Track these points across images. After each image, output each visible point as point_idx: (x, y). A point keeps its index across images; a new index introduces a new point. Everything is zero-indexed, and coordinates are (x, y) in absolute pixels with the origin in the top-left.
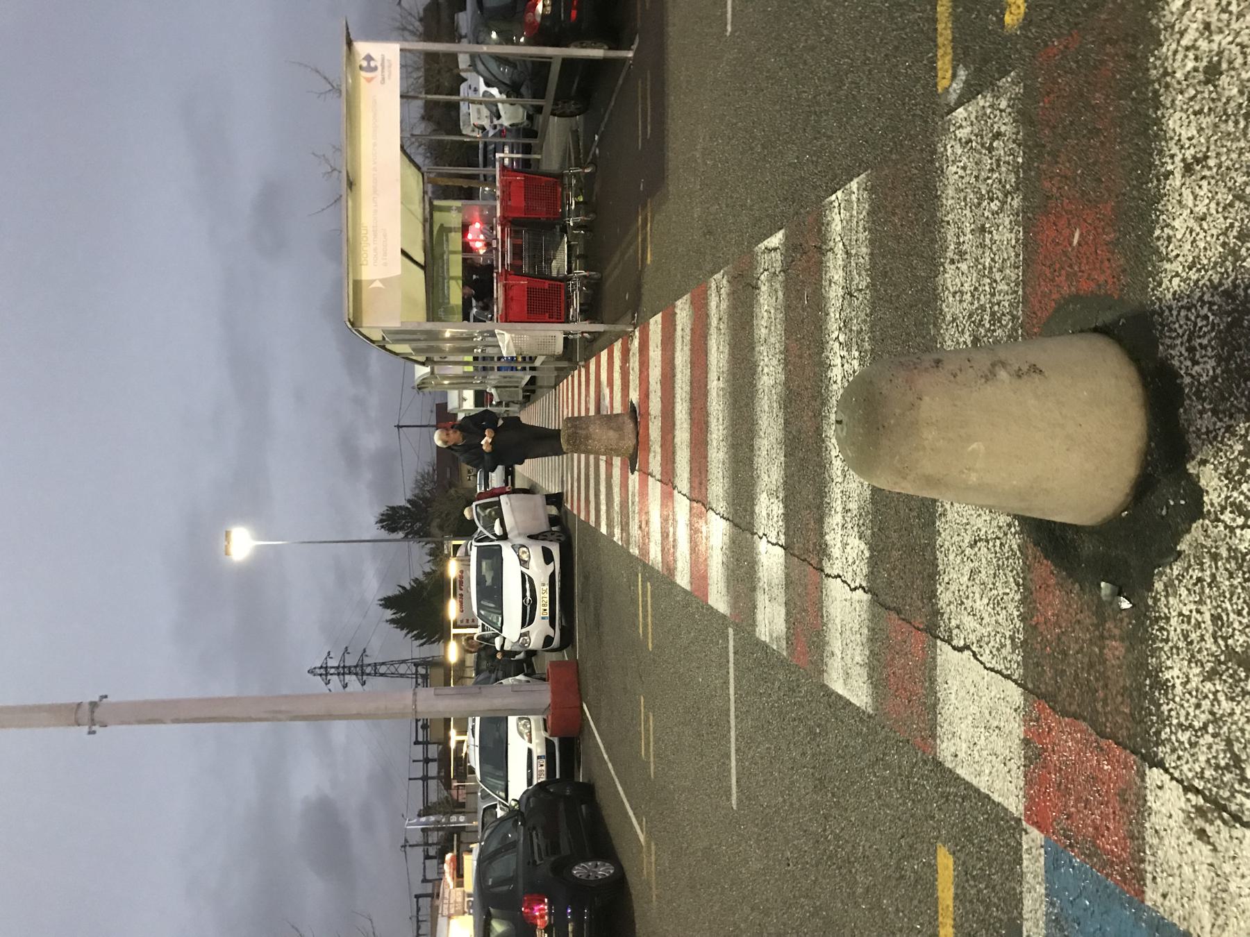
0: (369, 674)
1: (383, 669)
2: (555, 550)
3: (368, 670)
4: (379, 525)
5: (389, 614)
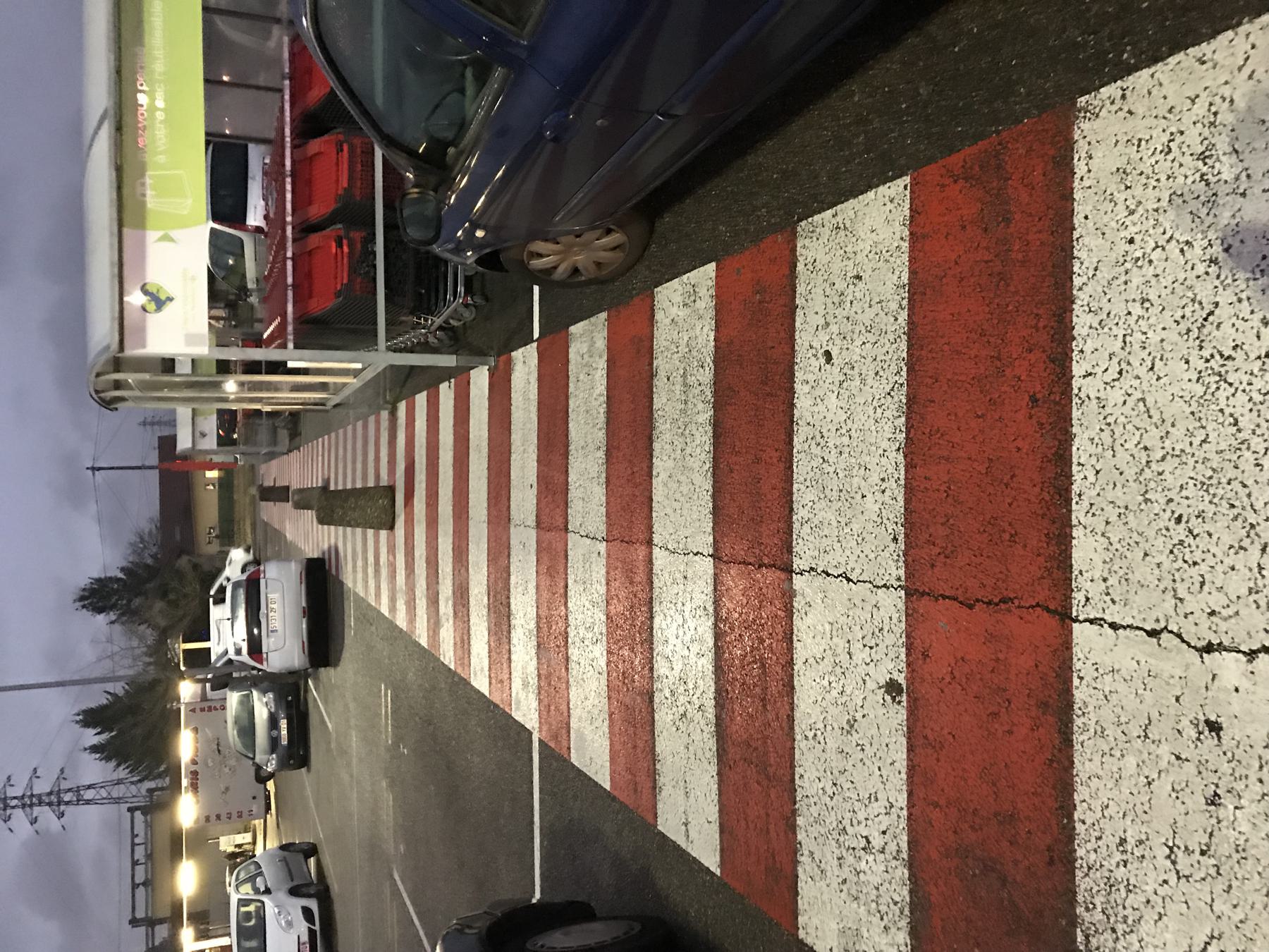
0: (67, 803)
1: (89, 795)
2: (313, 905)
3: (67, 797)
4: (78, 604)
5: (91, 737)
